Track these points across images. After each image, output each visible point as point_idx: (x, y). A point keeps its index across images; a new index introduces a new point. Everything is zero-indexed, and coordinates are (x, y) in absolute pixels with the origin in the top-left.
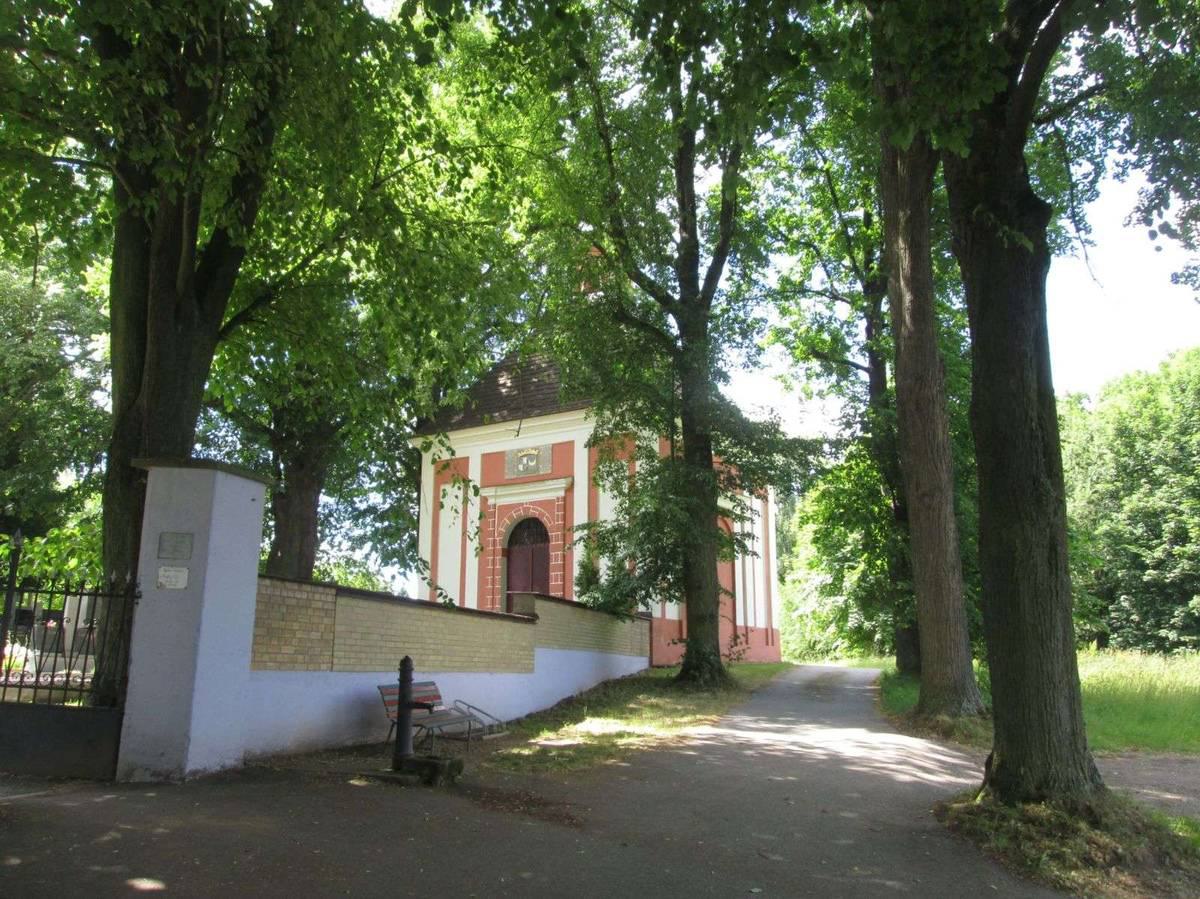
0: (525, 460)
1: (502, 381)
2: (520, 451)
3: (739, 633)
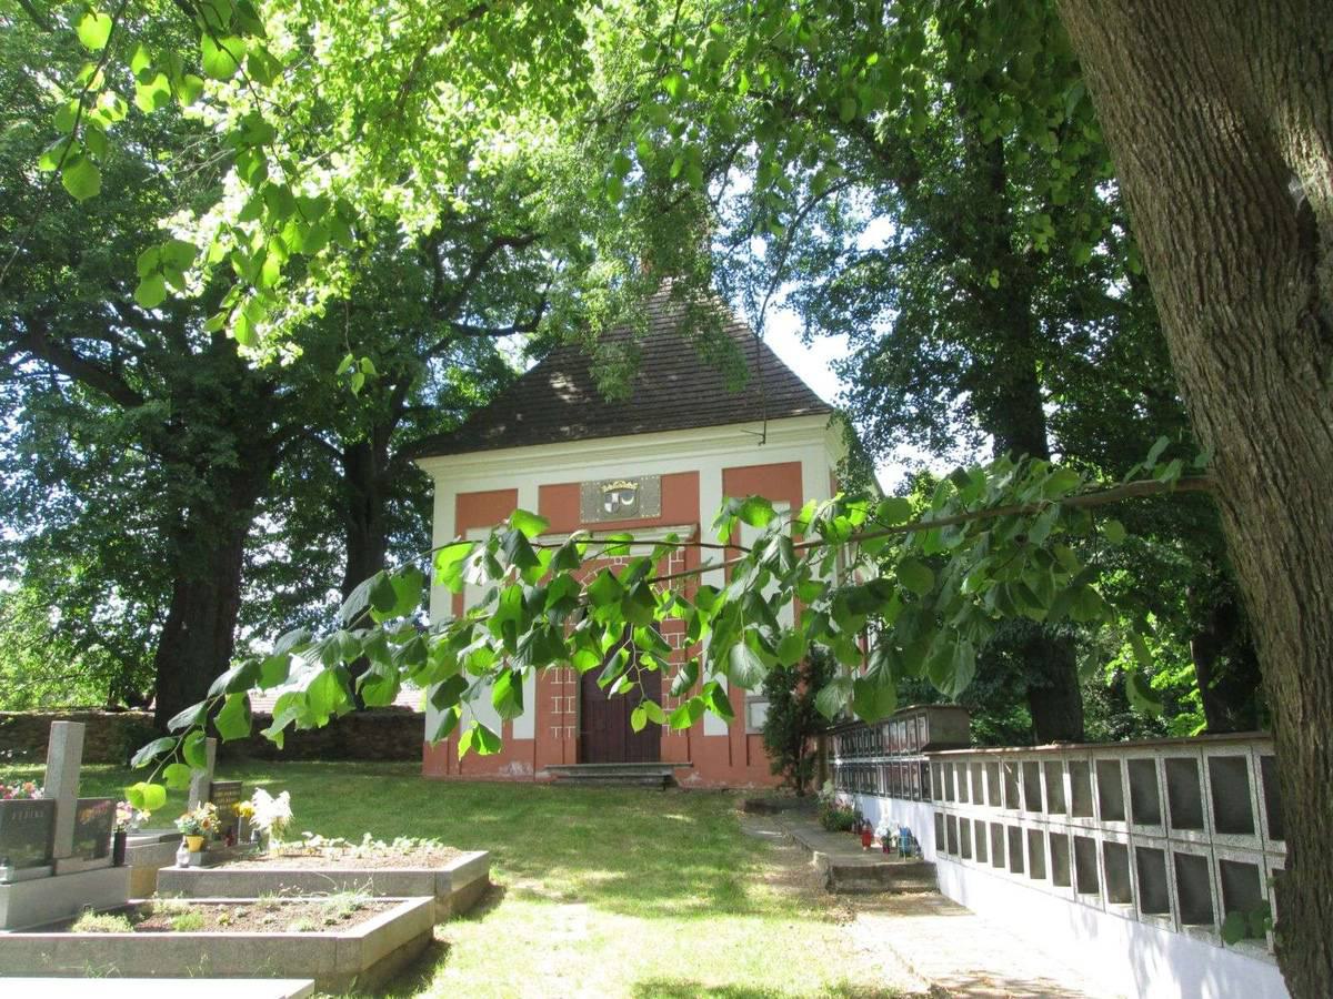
0: (615, 497)
1: (558, 384)
2: (606, 483)
3: (1283, 59)
